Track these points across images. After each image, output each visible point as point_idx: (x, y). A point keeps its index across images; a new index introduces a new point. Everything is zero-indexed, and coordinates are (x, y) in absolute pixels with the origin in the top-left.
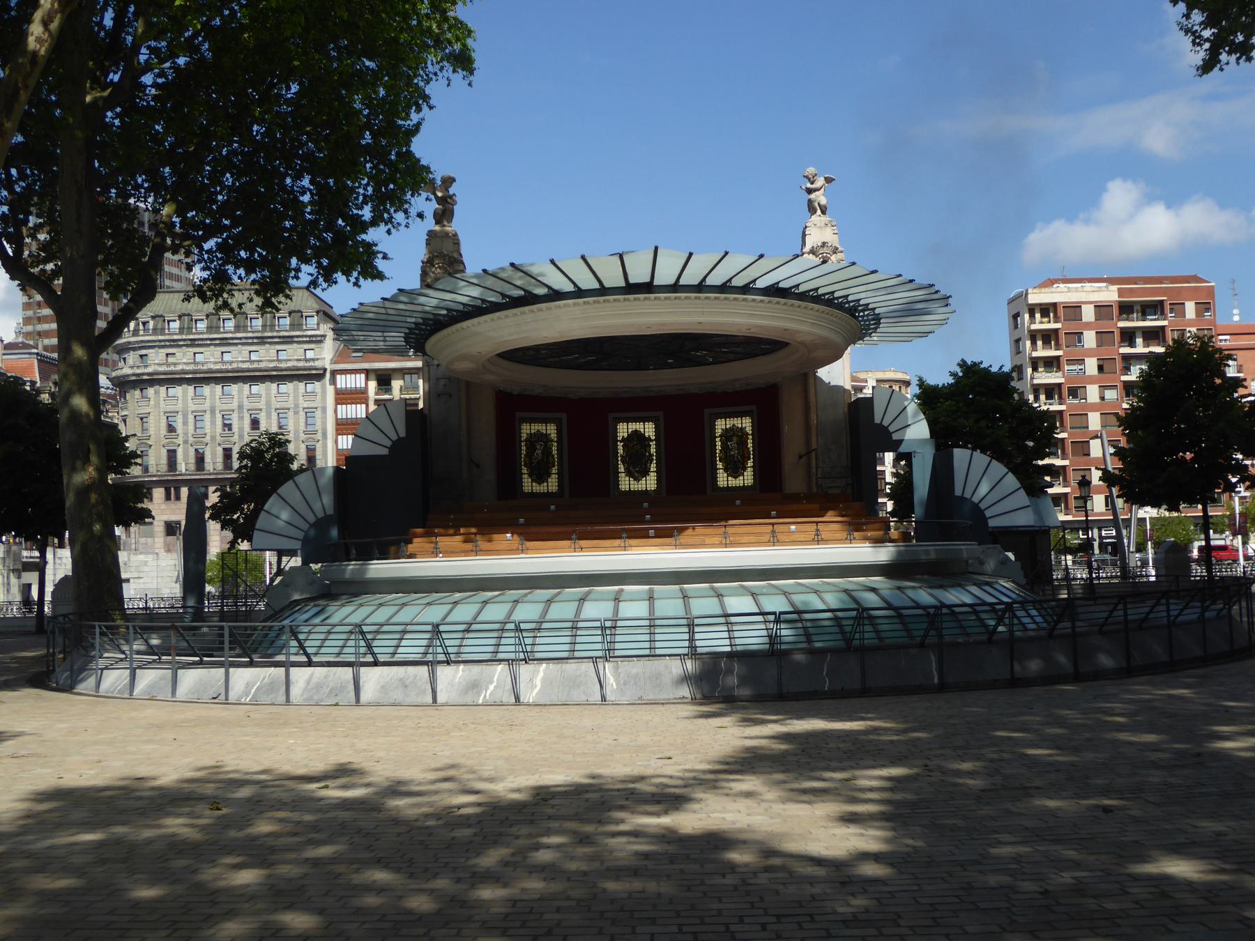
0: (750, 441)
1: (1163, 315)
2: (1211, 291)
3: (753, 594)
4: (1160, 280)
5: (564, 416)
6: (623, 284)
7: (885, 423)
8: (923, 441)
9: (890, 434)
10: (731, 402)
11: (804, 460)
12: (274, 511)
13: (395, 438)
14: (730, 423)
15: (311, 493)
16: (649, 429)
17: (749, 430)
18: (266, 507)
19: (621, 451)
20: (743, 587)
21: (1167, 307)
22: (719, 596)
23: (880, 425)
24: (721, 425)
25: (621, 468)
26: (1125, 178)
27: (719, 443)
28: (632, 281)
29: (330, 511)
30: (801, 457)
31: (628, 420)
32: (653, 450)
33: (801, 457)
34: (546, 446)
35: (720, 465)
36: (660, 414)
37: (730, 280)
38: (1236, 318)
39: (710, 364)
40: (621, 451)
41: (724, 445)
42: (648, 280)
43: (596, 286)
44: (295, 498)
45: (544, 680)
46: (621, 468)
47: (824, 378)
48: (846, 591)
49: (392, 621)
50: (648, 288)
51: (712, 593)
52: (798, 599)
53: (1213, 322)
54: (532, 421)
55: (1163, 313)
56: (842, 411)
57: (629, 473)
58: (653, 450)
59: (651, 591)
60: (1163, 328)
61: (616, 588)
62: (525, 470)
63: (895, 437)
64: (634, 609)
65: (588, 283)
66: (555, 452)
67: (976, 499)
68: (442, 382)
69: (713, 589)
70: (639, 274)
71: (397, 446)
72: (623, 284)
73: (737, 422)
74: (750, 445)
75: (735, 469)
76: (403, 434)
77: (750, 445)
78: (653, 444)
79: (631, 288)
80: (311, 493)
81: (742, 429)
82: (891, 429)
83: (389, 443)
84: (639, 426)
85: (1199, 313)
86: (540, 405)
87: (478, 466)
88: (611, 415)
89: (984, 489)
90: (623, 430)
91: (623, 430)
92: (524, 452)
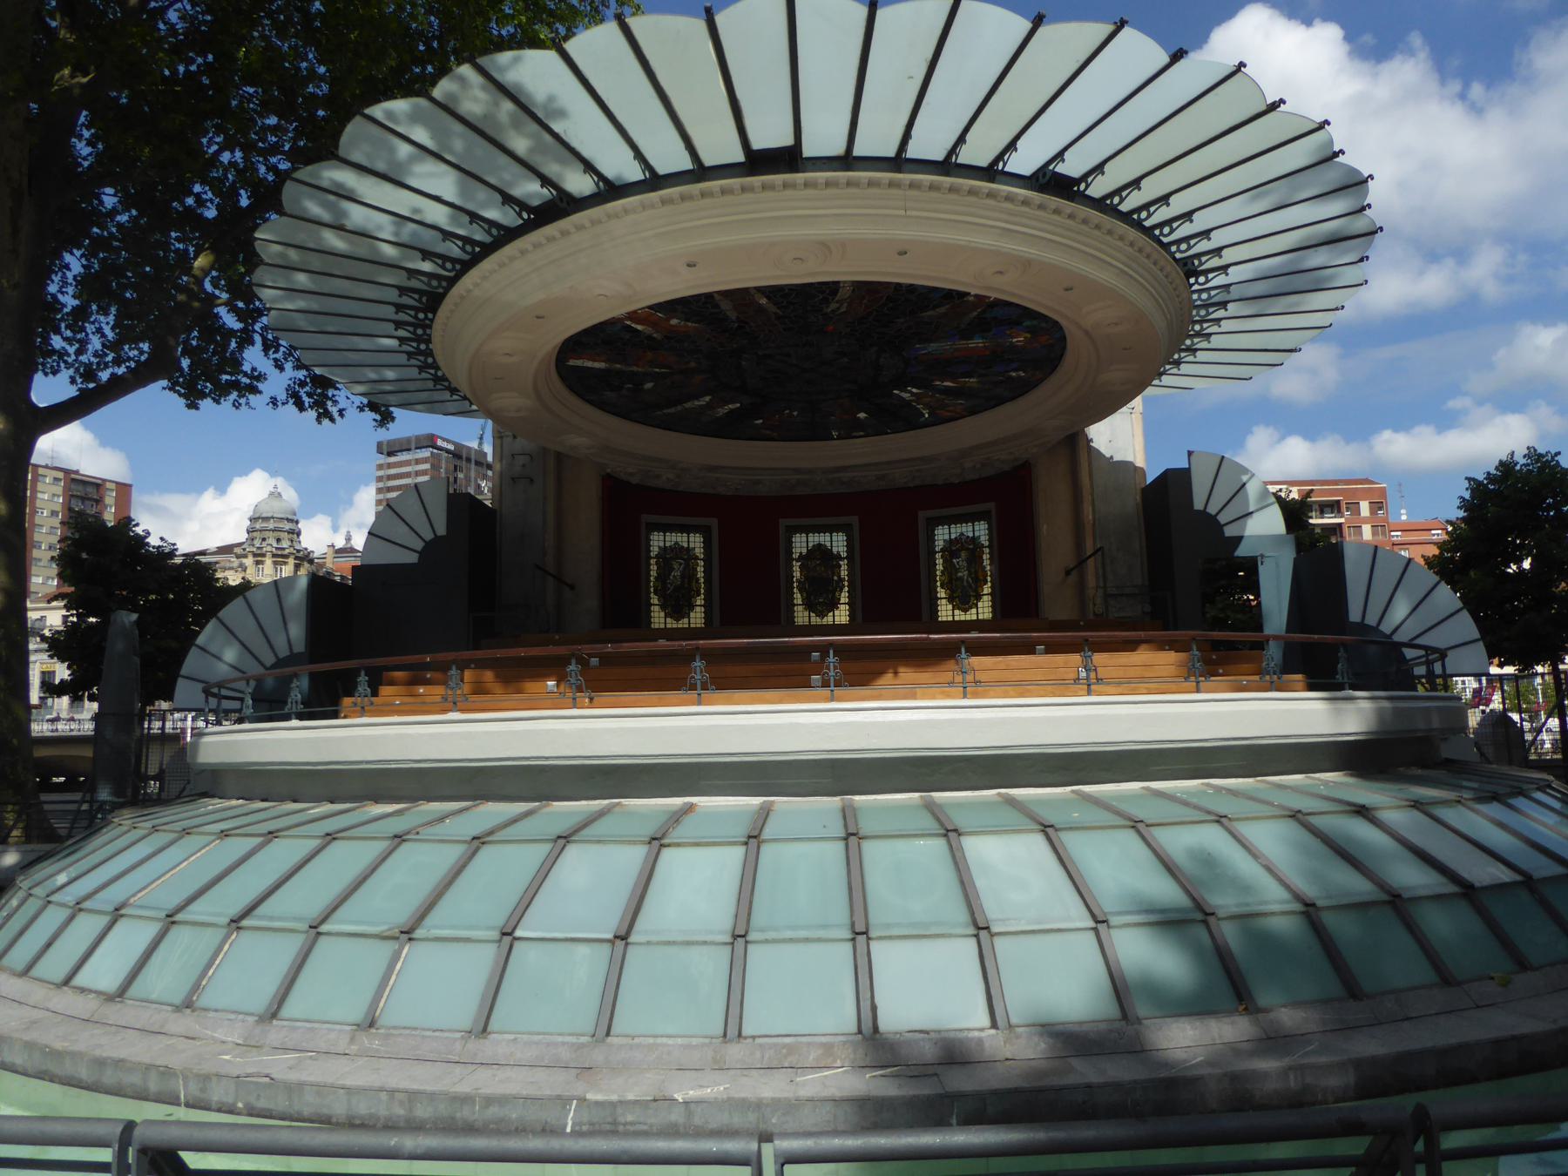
0: (986, 557)
1: (1339, 513)
2: (1383, 491)
3: (1046, 829)
4: (1336, 482)
5: (713, 522)
6: (739, 157)
7: (1212, 510)
8: (1275, 539)
9: (1220, 527)
10: (956, 497)
11: (1073, 577)
12: (213, 649)
13: (429, 536)
14: (956, 530)
15: (271, 620)
16: (838, 543)
17: (984, 540)
18: (200, 640)
19: (797, 574)
20: (1012, 802)
21: (1344, 506)
22: (950, 833)
23: (1204, 513)
24: (657, 541)
25: (798, 598)
26: (1267, 425)
27: (939, 561)
28: (757, 144)
29: (299, 647)
30: (1068, 573)
31: (807, 530)
32: (844, 573)
33: (1068, 573)
34: (687, 565)
35: (942, 593)
36: (854, 520)
37: (1060, 156)
38: (1404, 518)
39: (927, 425)
40: (797, 574)
41: (949, 568)
42: (787, 140)
43: (686, 164)
44: (247, 628)
45: (732, 411)
46: (798, 598)
47: (1103, 450)
48: (1295, 815)
49: (1417, 642)
50: (788, 159)
51: (929, 823)
52: (1180, 841)
53: (1386, 520)
54: (665, 528)
55: (1339, 511)
56: (1133, 501)
57: (809, 606)
58: (844, 573)
59: (765, 813)
60: (1340, 525)
61: (678, 802)
62: (655, 600)
63: (1229, 532)
64: (696, 884)
65: (669, 157)
66: (700, 575)
67: (1386, 628)
68: (521, 460)
69: (932, 809)
70: (770, 133)
71: (432, 549)
72: (739, 157)
73: (967, 529)
74: (986, 562)
75: (964, 599)
76: (442, 530)
77: (986, 562)
78: (844, 564)
79: (759, 162)
80: (271, 620)
81: (974, 540)
82: (1222, 519)
83: (419, 545)
84: (824, 539)
85: (1373, 512)
86: (680, 505)
87: (572, 587)
88: (784, 522)
89: (1400, 610)
90: (801, 544)
91: (801, 544)
92: (654, 573)
